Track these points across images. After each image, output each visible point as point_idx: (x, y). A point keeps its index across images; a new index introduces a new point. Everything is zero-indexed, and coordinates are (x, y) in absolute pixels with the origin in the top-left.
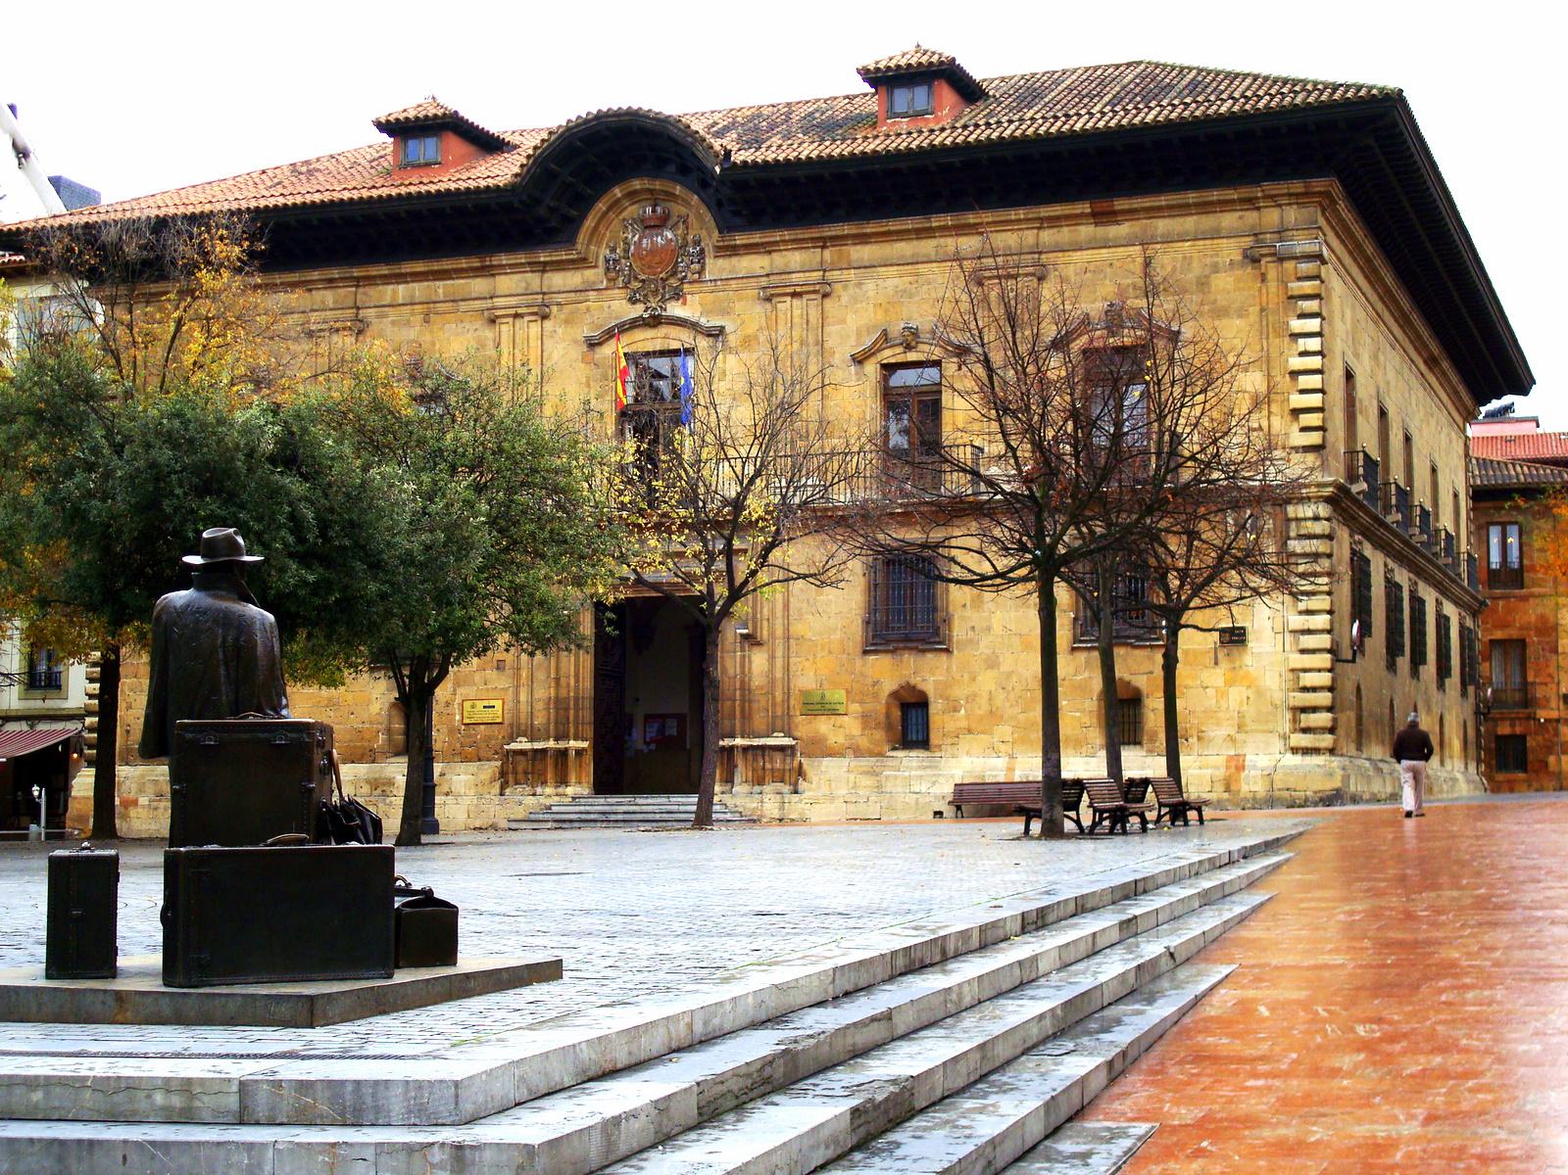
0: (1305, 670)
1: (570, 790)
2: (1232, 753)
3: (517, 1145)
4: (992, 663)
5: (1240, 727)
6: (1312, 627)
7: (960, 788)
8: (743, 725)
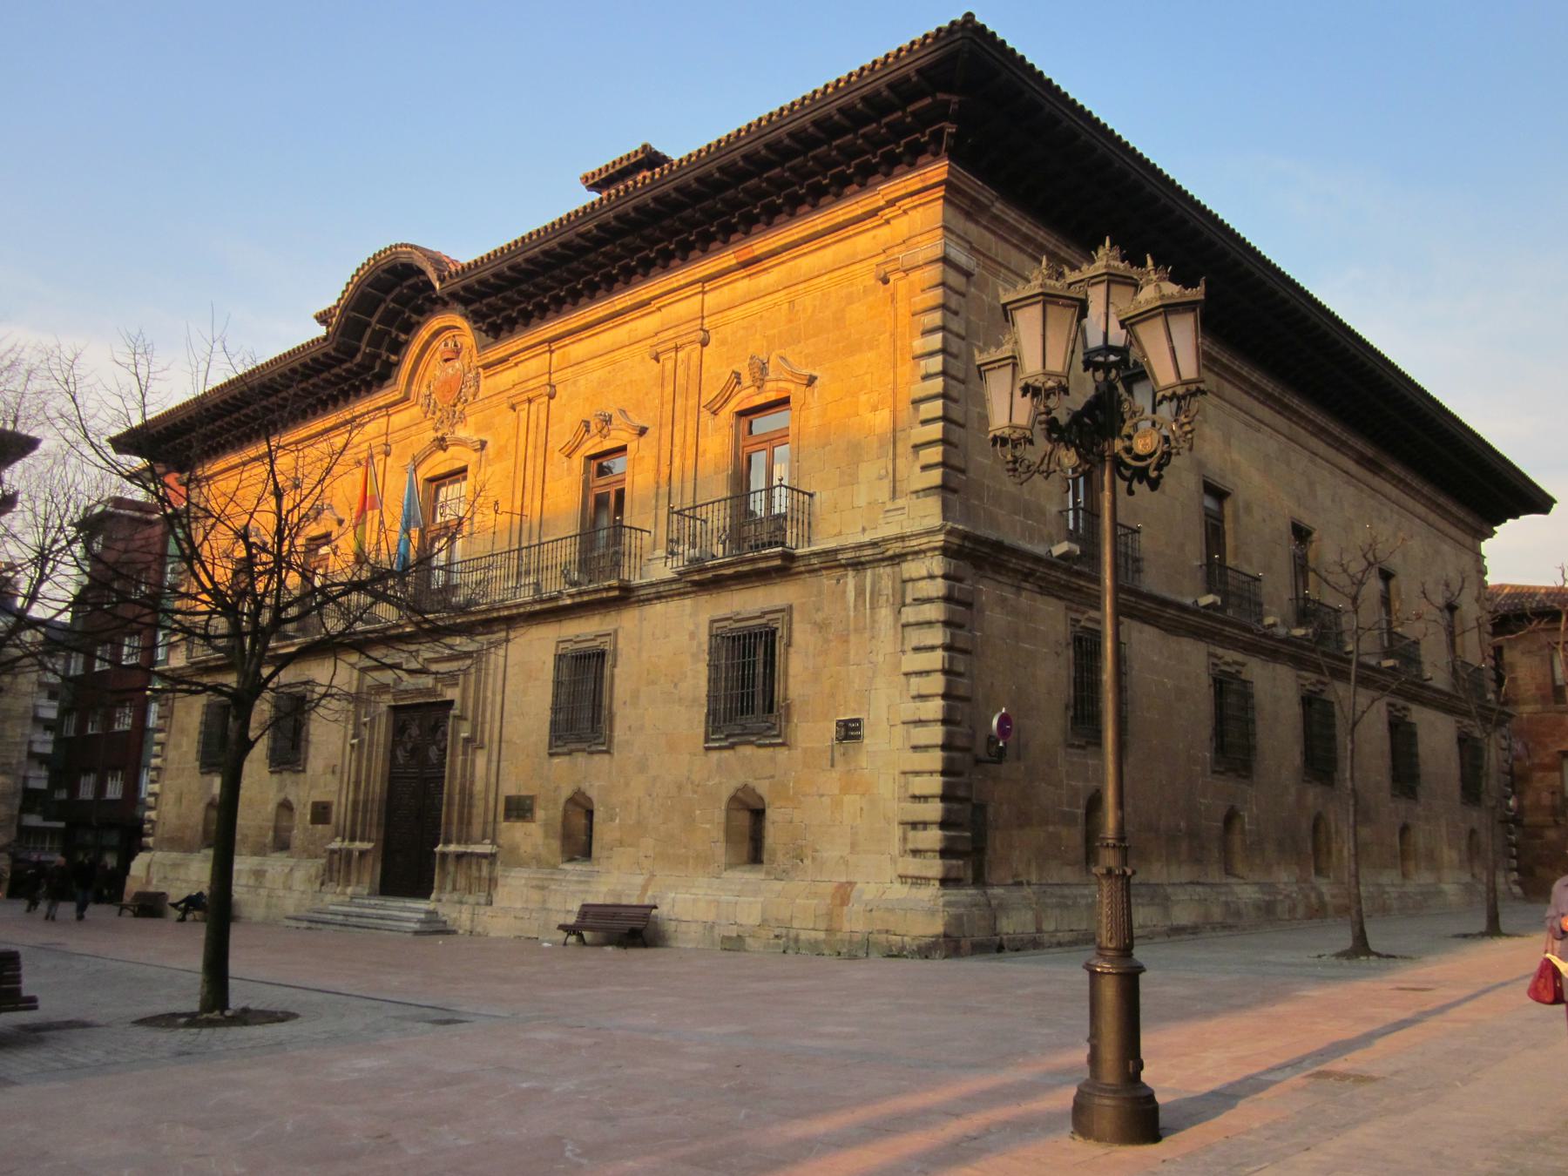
0: (917, 773)
1: (349, 890)
2: (843, 879)
3: (1508, 935)
4: (642, 767)
5: (854, 846)
6: (923, 717)
7: (586, 911)
8: (460, 830)
